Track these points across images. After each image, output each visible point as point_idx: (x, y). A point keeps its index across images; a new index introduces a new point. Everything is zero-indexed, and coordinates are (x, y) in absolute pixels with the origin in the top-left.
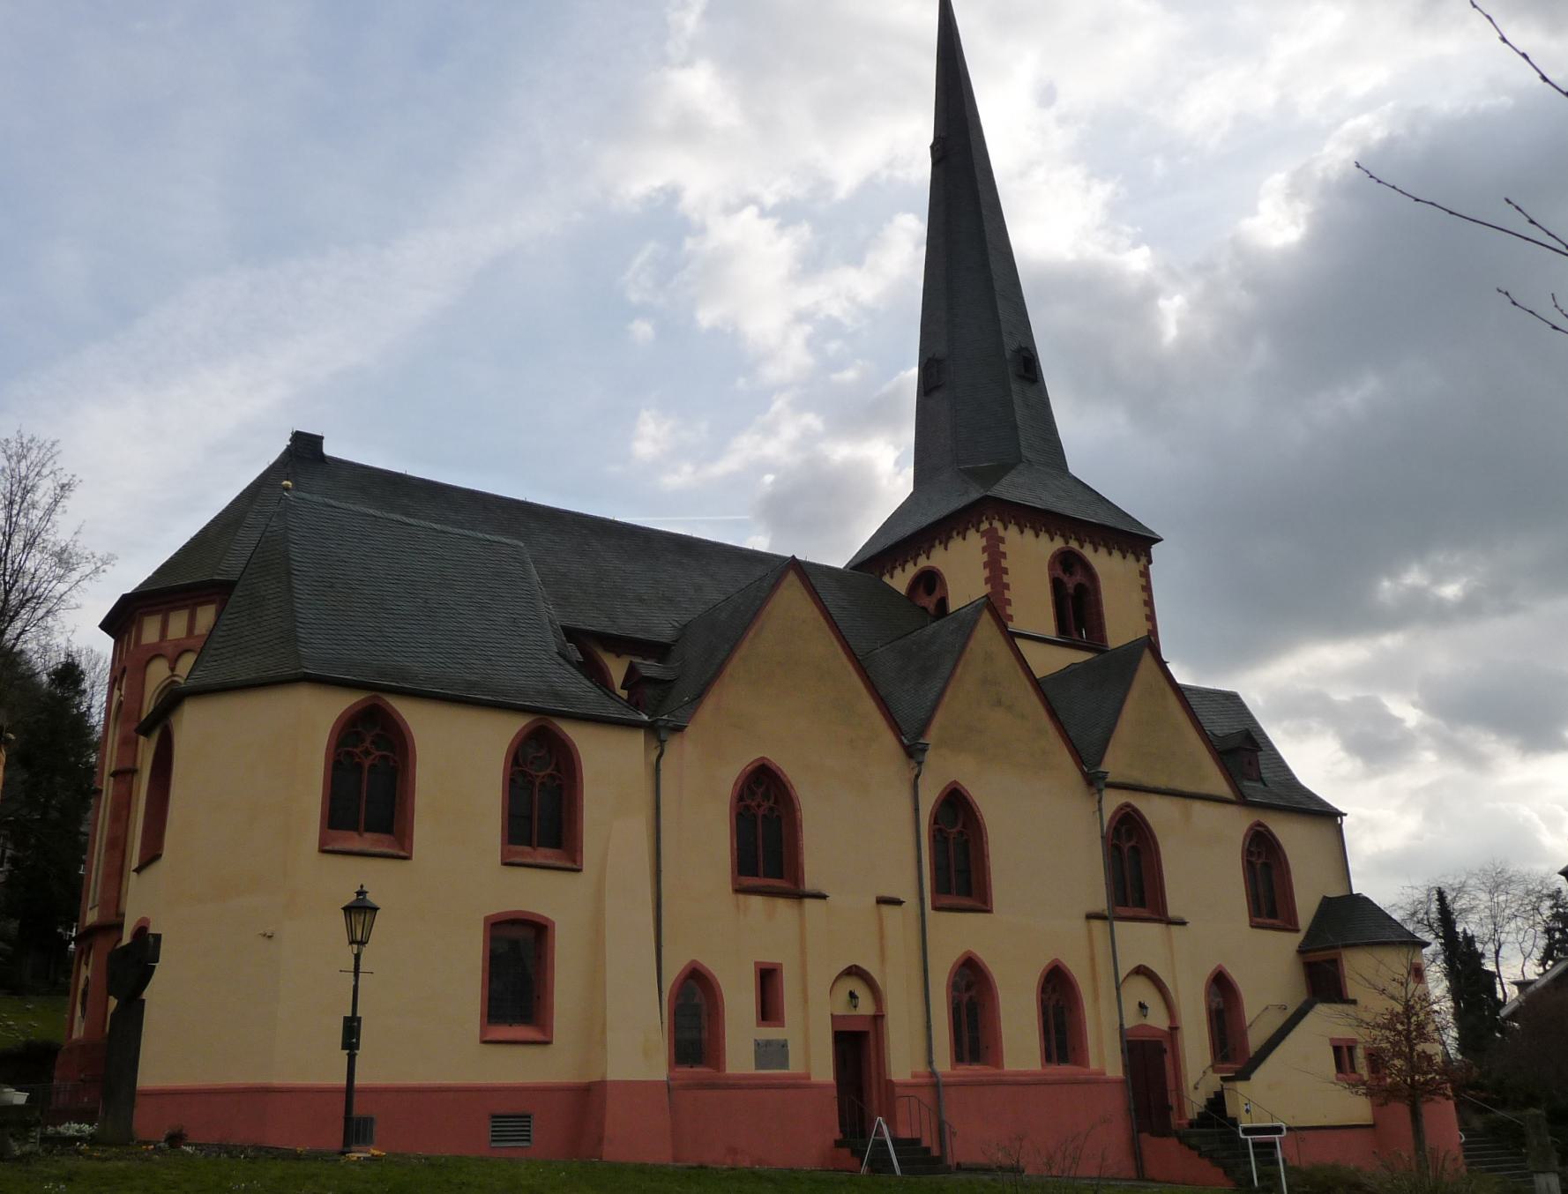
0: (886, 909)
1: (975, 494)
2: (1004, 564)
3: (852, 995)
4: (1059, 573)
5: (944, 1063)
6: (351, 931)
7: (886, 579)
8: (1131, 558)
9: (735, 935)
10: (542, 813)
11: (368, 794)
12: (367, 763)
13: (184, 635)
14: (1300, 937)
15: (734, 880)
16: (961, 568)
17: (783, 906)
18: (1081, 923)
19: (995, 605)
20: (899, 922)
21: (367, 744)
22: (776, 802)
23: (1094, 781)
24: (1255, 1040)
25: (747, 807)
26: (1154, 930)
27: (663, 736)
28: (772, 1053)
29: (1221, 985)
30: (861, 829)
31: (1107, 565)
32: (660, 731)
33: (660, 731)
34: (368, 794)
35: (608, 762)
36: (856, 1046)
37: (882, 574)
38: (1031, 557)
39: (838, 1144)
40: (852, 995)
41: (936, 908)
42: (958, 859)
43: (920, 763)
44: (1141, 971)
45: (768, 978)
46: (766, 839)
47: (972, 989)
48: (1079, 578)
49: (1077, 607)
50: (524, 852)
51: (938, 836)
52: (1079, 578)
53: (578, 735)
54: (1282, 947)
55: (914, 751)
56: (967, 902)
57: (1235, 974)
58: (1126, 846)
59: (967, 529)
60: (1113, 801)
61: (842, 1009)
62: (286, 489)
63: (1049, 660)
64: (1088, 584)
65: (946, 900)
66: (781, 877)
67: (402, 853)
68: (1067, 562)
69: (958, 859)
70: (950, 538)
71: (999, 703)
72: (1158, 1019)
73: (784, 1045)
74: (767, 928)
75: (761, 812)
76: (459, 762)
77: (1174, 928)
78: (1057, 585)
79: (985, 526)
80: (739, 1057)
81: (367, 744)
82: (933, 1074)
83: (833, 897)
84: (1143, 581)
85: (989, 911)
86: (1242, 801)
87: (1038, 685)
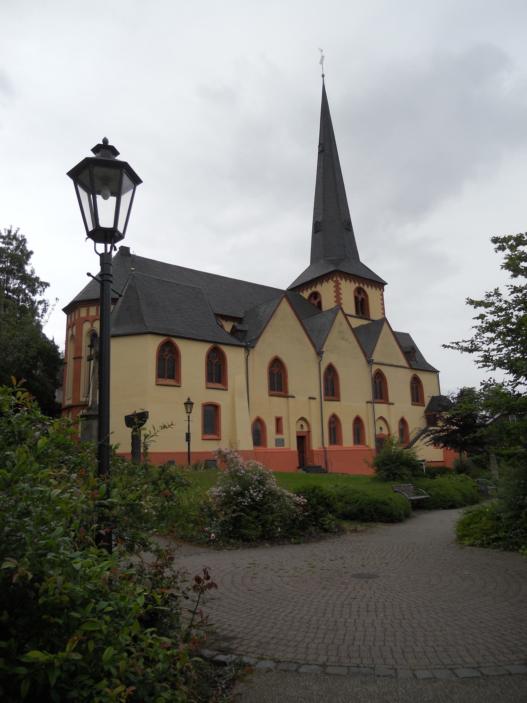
0: (311, 400)
1: (332, 269)
2: (341, 291)
3: (301, 425)
4: (357, 294)
5: (327, 444)
6: (187, 409)
7: (301, 293)
8: (378, 289)
9: (270, 408)
10: (216, 373)
11: (168, 368)
12: (167, 358)
13: (95, 314)
14: (425, 408)
15: (156, 381)
16: (326, 291)
17: (283, 400)
18: (365, 403)
19: (339, 307)
20: (315, 404)
21: (167, 352)
22: (280, 369)
23: (370, 362)
24: (412, 437)
25: (272, 370)
26: (385, 406)
27: (249, 349)
28: (280, 442)
29: (403, 422)
30: (304, 379)
31: (371, 292)
32: (248, 347)
33: (248, 347)
34: (168, 368)
35: (234, 357)
36: (302, 440)
37: (300, 292)
38: (348, 289)
39: (298, 468)
40: (301, 425)
41: (325, 400)
42: (331, 385)
43: (321, 357)
44: (381, 418)
45: (278, 420)
46: (278, 379)
47: (335, 423)
48: (362, 296)
49: (362, 306)
50: (162, 381)
51: (326, 379)
52: (362, 296)
53: (224, 348)
54: (420, 411)
55: (319, 354)
56: (333, 398)
57: (407, 419)
58: (378, 381)
59: (329, 279)
60: (375, 368)
61: (299, 430)
62: (133, 270)
63: (356, 323)
64: (365, 298)
65: (328, 398)
66: (281, 391)
67: (177, 385)
68: (359, 291)
69: (331, 385)
70: (323, 282)
71: (343, 338)
72: (385, 432)
73: (283, 440)
74: (277, 406)
75: (276, 372)
76: (193, 357)
77: (390, 405)
78: (356, 298)
79: (335, 279)
80: (271, 444)
81: (167, 352)
82: (324, 447)
83: (297, 398)
84: (381, 297)
85: (339, 401)
86: (411, 368)
87: (355, 331)
